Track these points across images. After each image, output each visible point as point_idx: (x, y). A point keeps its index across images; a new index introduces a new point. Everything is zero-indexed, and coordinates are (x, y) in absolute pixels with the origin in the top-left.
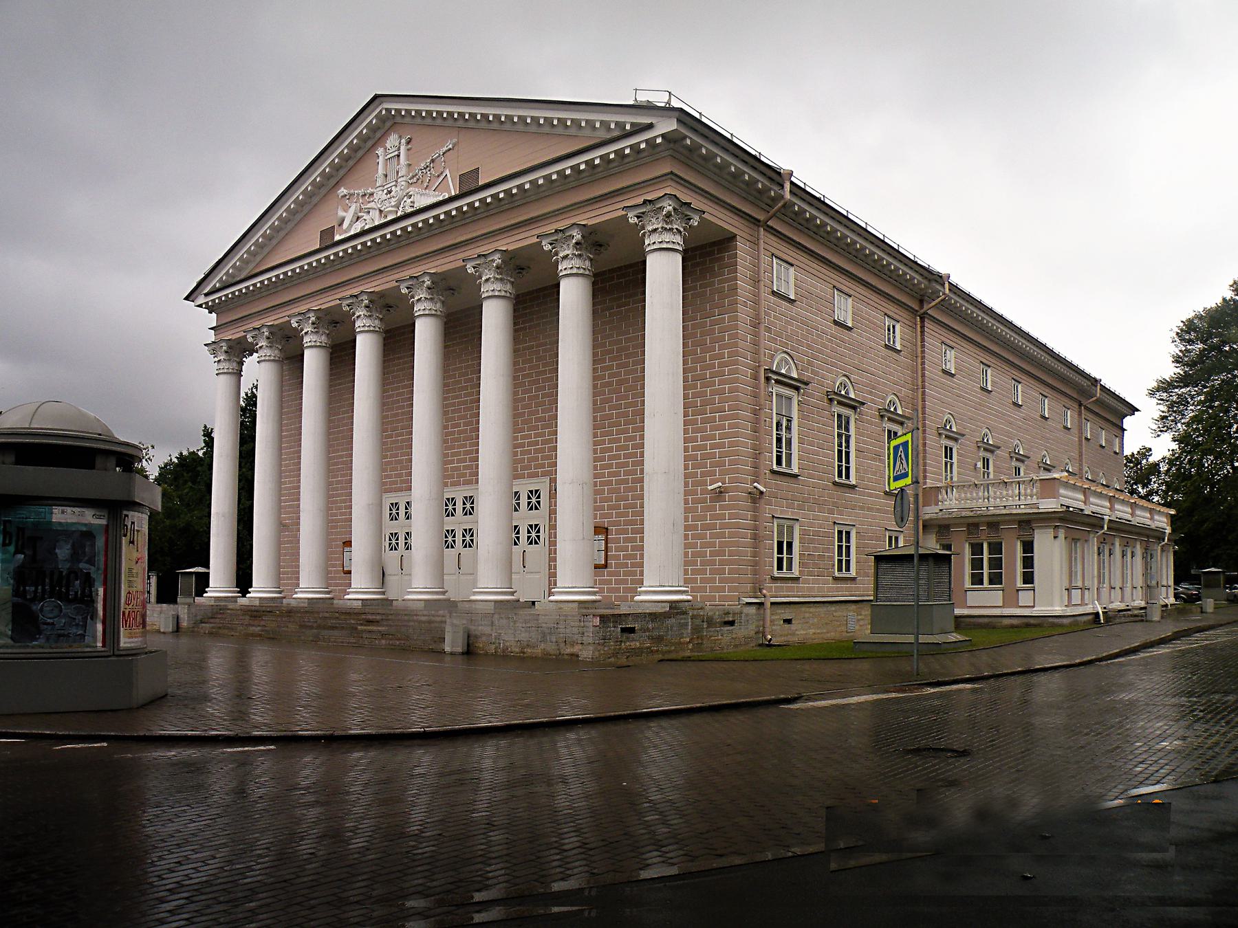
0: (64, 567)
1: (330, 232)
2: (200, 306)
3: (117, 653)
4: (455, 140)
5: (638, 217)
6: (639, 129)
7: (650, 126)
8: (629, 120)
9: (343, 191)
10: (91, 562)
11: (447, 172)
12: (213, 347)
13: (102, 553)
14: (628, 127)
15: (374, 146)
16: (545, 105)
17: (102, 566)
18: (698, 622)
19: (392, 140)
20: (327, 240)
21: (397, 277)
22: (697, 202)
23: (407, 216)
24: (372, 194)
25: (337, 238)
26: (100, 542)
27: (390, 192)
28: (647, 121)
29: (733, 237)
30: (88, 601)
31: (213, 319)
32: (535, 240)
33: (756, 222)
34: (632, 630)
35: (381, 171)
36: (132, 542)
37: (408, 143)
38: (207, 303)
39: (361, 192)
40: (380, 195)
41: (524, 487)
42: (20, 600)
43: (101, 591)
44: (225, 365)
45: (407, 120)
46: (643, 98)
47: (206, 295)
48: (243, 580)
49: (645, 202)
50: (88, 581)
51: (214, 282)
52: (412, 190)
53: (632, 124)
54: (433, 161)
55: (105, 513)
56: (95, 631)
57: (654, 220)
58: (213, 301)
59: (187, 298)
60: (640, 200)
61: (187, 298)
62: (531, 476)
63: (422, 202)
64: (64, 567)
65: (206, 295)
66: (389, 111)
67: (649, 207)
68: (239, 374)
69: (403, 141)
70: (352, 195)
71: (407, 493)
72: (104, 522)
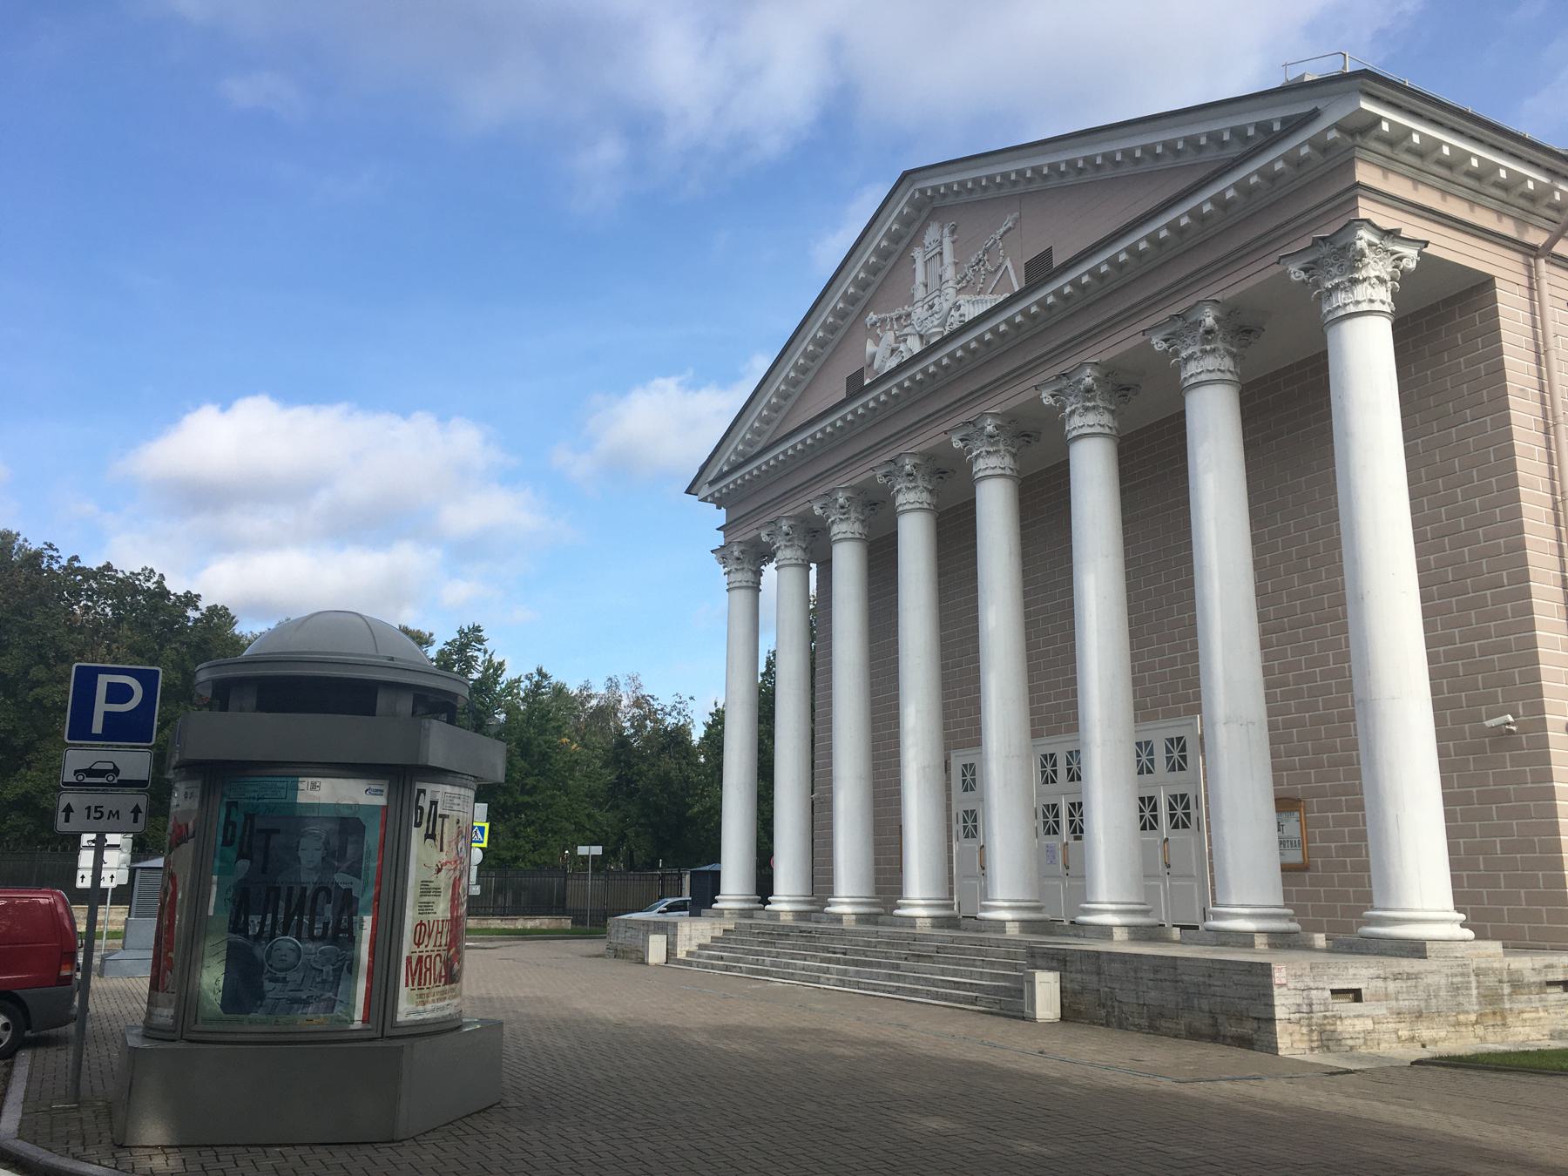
0: (309, 879)
1: (859, 374)
2: (704, 500)
3: (389, 1032)
4: (1016, 214)
5: (1306, 270)
6: (1294, 125)
7: (1314, 115)
8: (1275, 115)
9: (872, 317)
10: (355, 870)
11: (1008, 263)
12: (722, 553)
13: (375, 854)
14: (1277, 127)
15: (909, 247)
16: (1141, 127)
17: (373, 876)
18: (1491, 981)
19: (932, 233)
20: (856, 387)
21: (946, 427)
22: (1412, 227)
23: (954, 335)
24: (908, 315)
25: (867, 382)
26: (372, 838)
27: (931, 307)
28: (1305, 108)
29: (1484, 284)
30: (347, 937)
31: (721, 516)
32: (1140, 339)
33: (1531, 252)
34: (1357, 995)
35: (920, 277)
36: (430, 836)
37: (952, 232)
38: (712, 495)
39: (893, 315)
40: (919, 312)
41: (1159, 735)
42: (240, 939)
43: (368, 921)
44: (738, 576)
45: (949, 201)
46: (1293, 75)
47: (712, 483)
48: (764, 884)
49: (1316, 242)
50: (348, 904)
51: (722, 465)
52: (963, 298)
53: (1284, 121)
54: (987, 251)
55: (383, 786)
56: (352, 995)
57: (1334, 270)
58: (720, 491)
59: (688, 492)
60: (1307, 242)
61: (688, 492)
62: (1169, 714)
63: (971, 312)
64: (309, 879)
65: (712, 483)
66: (923, 191)
67: (1325, 250)
68: (756, 588)
69: (946, 231)
70: (884, 321)
71: (974, 750)
72: (381, 801)
